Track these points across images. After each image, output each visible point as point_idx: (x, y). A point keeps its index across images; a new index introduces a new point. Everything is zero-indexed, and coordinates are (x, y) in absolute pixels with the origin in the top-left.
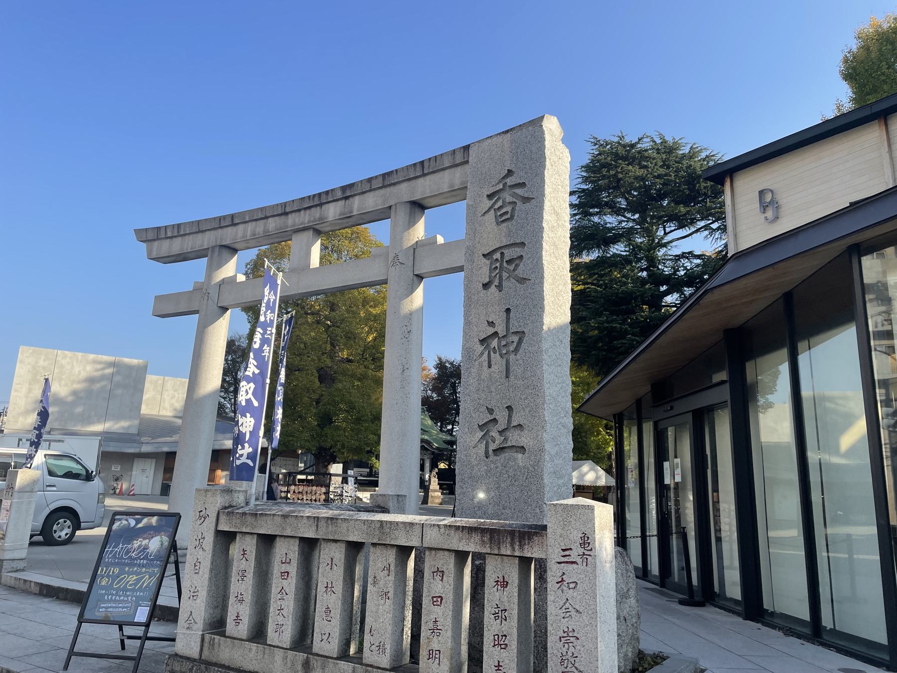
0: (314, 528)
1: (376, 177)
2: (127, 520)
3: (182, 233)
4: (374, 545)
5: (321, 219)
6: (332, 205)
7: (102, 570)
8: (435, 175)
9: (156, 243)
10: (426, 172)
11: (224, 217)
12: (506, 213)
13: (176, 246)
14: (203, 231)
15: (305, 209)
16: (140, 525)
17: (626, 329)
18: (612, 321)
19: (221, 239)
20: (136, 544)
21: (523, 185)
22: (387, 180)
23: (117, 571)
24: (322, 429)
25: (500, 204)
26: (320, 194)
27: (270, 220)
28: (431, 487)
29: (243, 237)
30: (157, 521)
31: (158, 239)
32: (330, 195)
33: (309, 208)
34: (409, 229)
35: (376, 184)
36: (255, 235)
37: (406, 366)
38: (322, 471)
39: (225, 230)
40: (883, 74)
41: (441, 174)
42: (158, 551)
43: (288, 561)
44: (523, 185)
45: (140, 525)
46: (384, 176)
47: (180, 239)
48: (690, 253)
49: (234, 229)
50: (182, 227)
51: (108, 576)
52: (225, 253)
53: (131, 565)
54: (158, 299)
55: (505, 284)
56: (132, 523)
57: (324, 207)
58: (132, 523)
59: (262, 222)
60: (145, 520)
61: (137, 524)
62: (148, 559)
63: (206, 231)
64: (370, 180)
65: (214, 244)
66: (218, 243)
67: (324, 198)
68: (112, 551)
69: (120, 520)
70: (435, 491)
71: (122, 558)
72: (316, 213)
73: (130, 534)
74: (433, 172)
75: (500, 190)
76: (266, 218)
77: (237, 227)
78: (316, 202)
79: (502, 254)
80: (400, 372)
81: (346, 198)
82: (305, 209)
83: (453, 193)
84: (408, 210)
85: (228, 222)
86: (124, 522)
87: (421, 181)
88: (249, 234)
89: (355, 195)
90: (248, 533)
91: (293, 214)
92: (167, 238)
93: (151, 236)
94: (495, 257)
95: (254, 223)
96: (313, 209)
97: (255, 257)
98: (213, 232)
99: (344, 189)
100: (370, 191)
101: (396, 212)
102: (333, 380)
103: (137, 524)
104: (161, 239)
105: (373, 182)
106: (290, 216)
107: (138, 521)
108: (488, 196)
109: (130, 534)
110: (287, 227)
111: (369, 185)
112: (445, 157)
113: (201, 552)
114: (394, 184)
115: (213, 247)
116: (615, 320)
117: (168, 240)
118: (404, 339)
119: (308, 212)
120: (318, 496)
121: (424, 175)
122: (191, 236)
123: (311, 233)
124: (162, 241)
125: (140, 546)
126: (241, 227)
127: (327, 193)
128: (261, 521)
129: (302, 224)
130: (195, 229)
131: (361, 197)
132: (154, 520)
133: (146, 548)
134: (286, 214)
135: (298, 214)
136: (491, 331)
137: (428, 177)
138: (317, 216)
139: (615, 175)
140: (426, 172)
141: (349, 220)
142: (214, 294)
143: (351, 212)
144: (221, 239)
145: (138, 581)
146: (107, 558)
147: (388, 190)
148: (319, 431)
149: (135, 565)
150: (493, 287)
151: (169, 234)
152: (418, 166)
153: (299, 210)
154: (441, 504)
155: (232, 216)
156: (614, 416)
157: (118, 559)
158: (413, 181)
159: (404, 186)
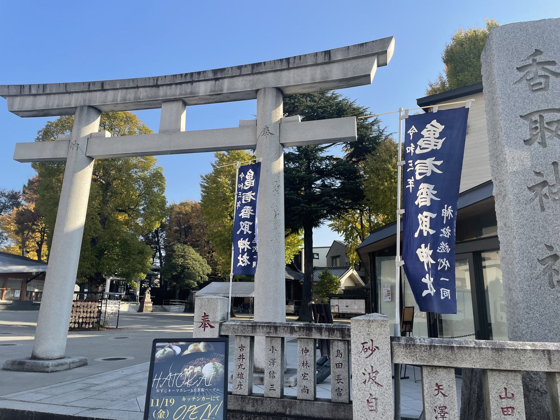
0: (546, 361)
1: (246, 66)
2: (170, 347)
3: (48, 92)
4: (492, 370)
5: (191, 93)
6: (202, 84)
7: (155, 402)
8: (298, 70)
9: (18, 99)
10: (291, 66)
11: (94, 83)
12: (540, 84)
13: (28, 103)
14: (70, 93)
15: (176, 84)
16: (187, 352)
17: (299, 200)
18: (291, 194)
19: (90, 101)
20: (188, 371)
21: (553, 63)
22: (256, 69)
23: (173, 401)
24: (100, 259)
25: (531, 75)
26: (192, 74)
27: (141, 89)
28: (146, 300)
29: (113, 101)
30: (205, 347)
31: (21, 95)
32: (202, 75)
33: (181, 84)
34: (276, 108)
35: (244, 71)
36: (125, 100)
37: (277, 212)
38: (94, 291)
39: (94, 94)
40: (470, 61)
41: (303, 70)
42: (214, 378)
43: (509, 395)
44: (553, 63)
45: (187, 352)
46: (253, 66)
47: (45, 97)
48: (331, 156)
49: (103, 94)
50: (48, 87)
51: (164, 408)
52: (93, 112)
53: (186, 394)
54: (19, 145)
55: (548, 141)
56: (178, 350)
57: (195, 84)
58: (178, 350)
59: (132, 91)
60: (191, 347)
61: (183, 351)
62: (205, 388)
63: (73, 92)
64: (240, 67)
65: (82, 104)
66: (87, 103)
67: (196, 78)
68: (161, 382)
69: (162, 347)
70: (149, 303)
71: (175, 387)
72: (188, 88)
73: (179, 362)
74: (297, 68)
75: (530, 65)
76: (137, 87)
77: (106, 92)
78: (188, 79)
79: (541, 117)
80: (273, 216)
81: (217, 79)
82: (176, 84)
83: (313, 85)
84: (275, 93)
85: (98, 87)
86: (168, 350)
87: (285, 73)
88: (119, 99)
89: (225, 78)
90: (440, 367)
91: (165, 87)
92: (30, 95)
93: (13, 91)
94: (534, 119)
95: (125, 91)
96: (184, 85)
97: (45, 127)
98: (80, 94)
99: (215, 72)
100: (239, 76)
101: (265, 94)
102: (129, 223)
103: (183, 351)
104: (23, 95)
105: (243, 69)
106: (161, 88)
107: (184, 348)
108: (517, 68)
109: (179, 362)
110: (159, 97)
111: (239, 71)
112: (308, 57)
113: (375, 387)
114: (261, 73)
115: (82, 107)
116: (291, 194)
117: (31, 97)
118: (275, 192)
119: (179, 86)
120: (92, 309)
121: (289, 69)
122: (57, 96)
123: (180, 103)
124: (24, 98)
125: (192, 374)
126: (111, 93)
127: (199, 73)
128: (459, 354)
129: (173, 95)
130: (62, 90)
131: (231, 80)
132: (201, 346)
133: (200, 375)
134: (157, 86)
135: (169, 87)
136: (540, 179)
137: (292, 71)
138: (189, 90)
139: (294, 103)
140: (291, 66)
141: (218, 96)
142: (83, 144)
143: (222, 90)
144: (90, 101)
145: (200, 411)
146: (158, 388)
147: (256, 77)
148: (98, 261)
149: (193, 394)
150: (536, 143)
151: (34, 91)
152: (284, 61)
153: (170, 85)
154: (152, 311)
155: (102, 83)
156: (369, 254)
157: (171, 388)
158: (279, 72)
159: (270, 75)
